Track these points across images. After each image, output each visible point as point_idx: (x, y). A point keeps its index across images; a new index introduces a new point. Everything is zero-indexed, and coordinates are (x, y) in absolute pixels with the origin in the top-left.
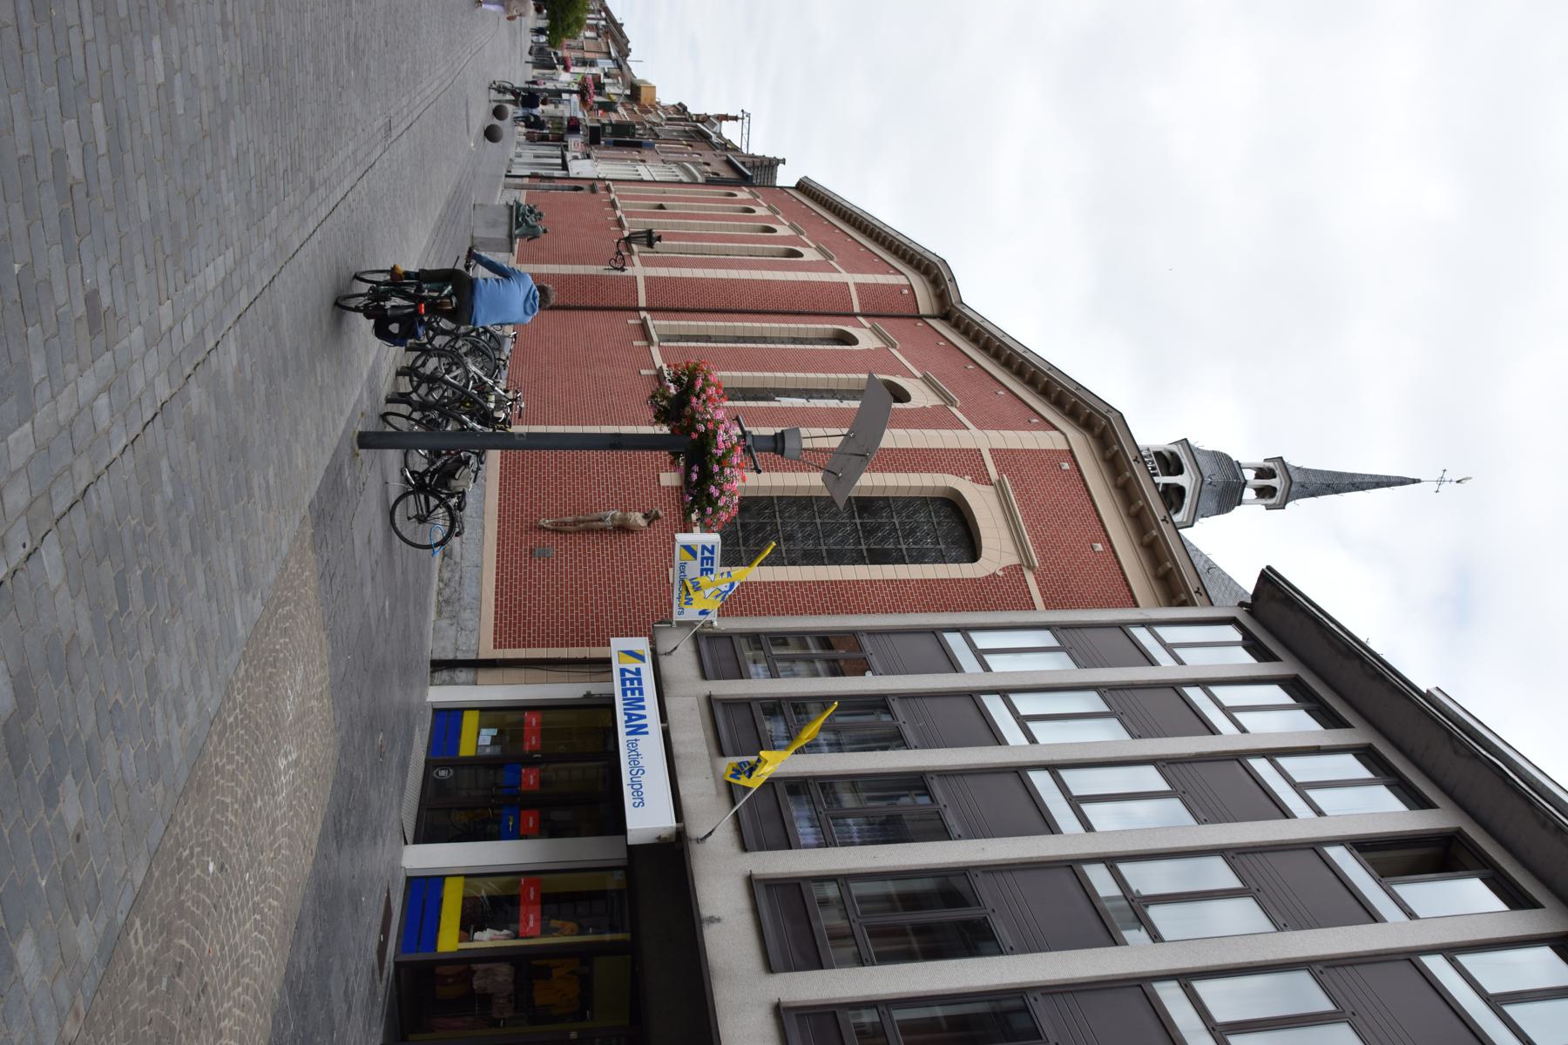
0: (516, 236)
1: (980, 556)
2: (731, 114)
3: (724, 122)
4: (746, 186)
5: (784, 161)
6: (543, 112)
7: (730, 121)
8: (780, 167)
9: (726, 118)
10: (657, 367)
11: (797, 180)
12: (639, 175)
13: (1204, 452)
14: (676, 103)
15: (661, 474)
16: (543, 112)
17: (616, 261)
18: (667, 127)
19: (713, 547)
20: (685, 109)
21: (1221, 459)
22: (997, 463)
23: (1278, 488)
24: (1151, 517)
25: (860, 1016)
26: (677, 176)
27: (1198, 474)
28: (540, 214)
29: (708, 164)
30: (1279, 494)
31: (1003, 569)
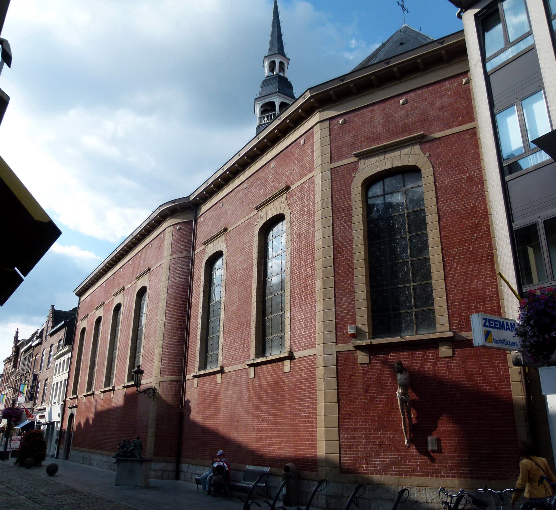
0: (141, 457)
1: (415, 166)
2: (14, 335)
3: (19, 339)
4: (77, 322)
5: (53, 306)
6: (198, 412)
7: (18, 336)
8: (56, 308)
9: (16, 337)
10: (354, 349)
11: (76, 296)
12: (61, 382)
13: (261, 91)
14: (3, 364)
15: (441, 356)
16: (198, 412)
17: (149, 394)
18: (20, 368)
19: (484, 319)
20: (9, 359)
21: (266, 82)
22: (340, 158)
23: (280, 60)
24: (403, 65)
25: (284, 354)
26: (64, 361)
27: (274, 94)
28: (125, 441)
29: (52, 345)
30: (283, 61)
31: (424, 153)
